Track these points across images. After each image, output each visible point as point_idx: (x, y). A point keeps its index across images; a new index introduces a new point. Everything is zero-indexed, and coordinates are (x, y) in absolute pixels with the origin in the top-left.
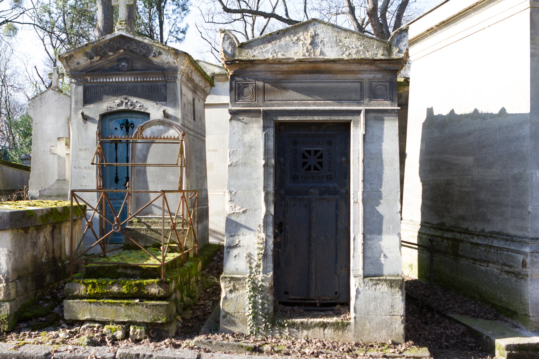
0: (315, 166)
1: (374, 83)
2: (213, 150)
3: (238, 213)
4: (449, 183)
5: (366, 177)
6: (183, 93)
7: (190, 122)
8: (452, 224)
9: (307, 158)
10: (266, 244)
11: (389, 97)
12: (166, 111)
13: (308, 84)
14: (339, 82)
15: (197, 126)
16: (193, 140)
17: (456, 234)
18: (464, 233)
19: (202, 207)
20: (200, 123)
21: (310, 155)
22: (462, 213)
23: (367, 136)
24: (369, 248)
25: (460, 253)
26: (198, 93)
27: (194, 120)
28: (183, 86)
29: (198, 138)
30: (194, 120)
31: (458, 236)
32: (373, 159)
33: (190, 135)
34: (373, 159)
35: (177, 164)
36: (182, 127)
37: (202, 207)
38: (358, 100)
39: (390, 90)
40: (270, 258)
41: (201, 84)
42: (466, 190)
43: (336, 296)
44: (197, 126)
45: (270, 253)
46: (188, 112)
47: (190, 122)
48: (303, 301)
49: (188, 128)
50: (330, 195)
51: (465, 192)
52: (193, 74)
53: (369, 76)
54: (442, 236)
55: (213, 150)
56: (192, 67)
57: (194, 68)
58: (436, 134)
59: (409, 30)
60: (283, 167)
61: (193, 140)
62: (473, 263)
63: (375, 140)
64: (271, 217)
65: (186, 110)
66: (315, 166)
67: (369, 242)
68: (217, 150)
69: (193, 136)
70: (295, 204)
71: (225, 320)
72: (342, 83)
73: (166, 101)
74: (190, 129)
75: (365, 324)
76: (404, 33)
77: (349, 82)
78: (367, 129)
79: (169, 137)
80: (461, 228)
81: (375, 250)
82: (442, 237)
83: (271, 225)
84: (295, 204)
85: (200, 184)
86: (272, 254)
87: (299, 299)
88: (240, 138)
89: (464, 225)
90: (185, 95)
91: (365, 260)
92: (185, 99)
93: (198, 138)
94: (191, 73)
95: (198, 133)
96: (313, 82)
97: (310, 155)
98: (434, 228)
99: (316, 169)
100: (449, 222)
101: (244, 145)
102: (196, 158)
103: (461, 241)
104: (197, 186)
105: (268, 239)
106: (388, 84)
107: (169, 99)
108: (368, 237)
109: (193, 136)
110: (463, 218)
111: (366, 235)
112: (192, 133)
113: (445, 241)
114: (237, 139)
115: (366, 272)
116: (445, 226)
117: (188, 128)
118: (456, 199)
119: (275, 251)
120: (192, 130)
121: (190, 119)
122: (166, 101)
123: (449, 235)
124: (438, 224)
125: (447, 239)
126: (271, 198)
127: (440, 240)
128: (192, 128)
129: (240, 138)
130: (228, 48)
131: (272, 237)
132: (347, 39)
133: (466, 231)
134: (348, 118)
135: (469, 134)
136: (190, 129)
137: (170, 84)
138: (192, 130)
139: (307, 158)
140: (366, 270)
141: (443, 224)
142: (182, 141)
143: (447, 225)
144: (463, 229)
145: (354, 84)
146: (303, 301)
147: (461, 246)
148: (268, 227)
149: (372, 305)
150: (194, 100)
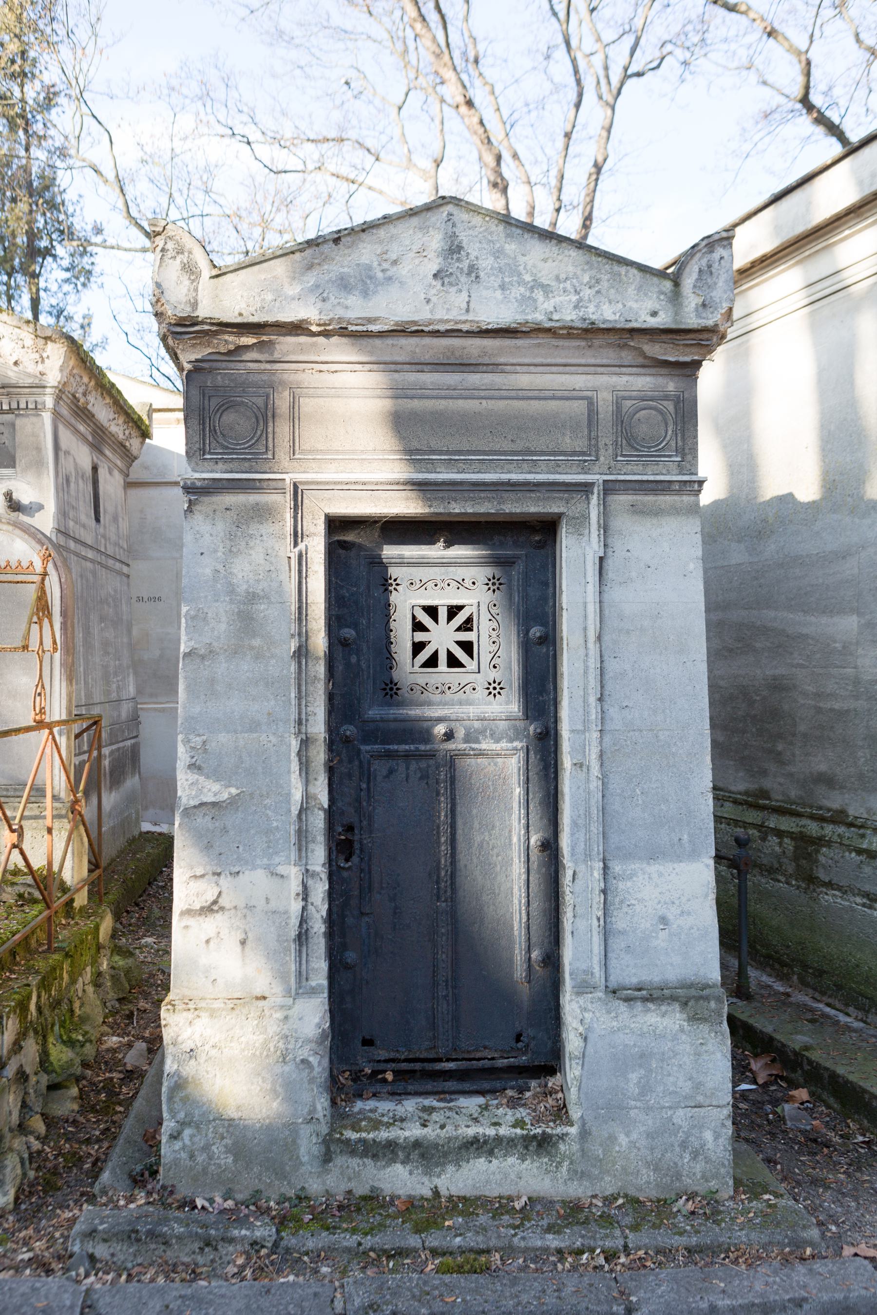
0: (450, 655)
1: (629, 403)
2: (150, 599)
3: (214, 804)
4: (778, 686)
5: (609, 687)
6: (64, 445)
7: (84, 526)
8: (793, 793)
9: (460, 643)
10: (305, 899)
11: (673, 443)
12: (15, 496)
13: (429, 404)
14: (523, 398)
15: (104, 536)
16: (94, 573)
17: (804, 821)
18: (833, 821)
19: (121, 745)
20: (113, 529)
21: (459, 629)
22: (823, 767)
23: (610, 564)
24: (622, 902)
25: (822, 875)
26: (107, 452)
27: (98, 520)
28: (61, 427)
29: (106, 567)
30: (98, 520)
31: (813, 828)
32: (628, 632)
33: (85, 558)
34: (628, 632)
35: (25, 648)
36: (62, 541)
37: (121, 745)
38: (583, 454)
39: (675, 423)
40: (319, 945)
41: (114, 429)
42: (837, 706)
43: (520, 1045)
44: (104, 536)
45: (318, 927)
46: (77, 499)
47: (84, 526)
48: (418, 1066)
49: (77, 541)
50: (497, 741)
51: (832, 710)
52: (91, 398)
53: (614, 379)
54: (762, 826)
55: (150, 599)
56: (86, 379)
57: (93, 383)
58: (738, 555)
59: (735, 242)
60: (354, 659)
61: (94, 573)
62: (864, 905)
63: (634, 574)
64: (321, 815)
65: (73, 493)
66: (450, 655)
67: (621, 885)
68: (159, 599)
69: (92, 561)
70: (391, 772)
71: (178, 1145)
72: (532, 402)
73: (14, 467)
74: (84, 544)
75: (612, 1138)
76: (720, 252)
77: (554, 398)
78: (609, 541)
79: (14, 564)
80: (820, 808)
81: (638, 908)
82: (760, 827)
83: (321, 838)
84: (391, 772)
85: (114, 686)
86: (323, 929)
87: (407, 1060)
88: (220, 567)
89: (834, 801)
90: (67, 453)
91: (610, 941)
92: (68, 465)
93: (106, 567)
94: (84, 394)
95: (108, 556)
96: (445, 398)
97: (459, 629)
98: (735, 802)
99: (453, 662)
100: (779, 786)
101: (231, 590)
102: (102, 619)
103: (820, 842)
104: (108, 692)
105: (310, 882)
106: (670, 406)
107: (21, 462)
108: (617, 867)
109: (92, 561)
110: (828, 781)
111: (610, 864)
112: (90, 554)
113: (773, 840)
114: (208, 571)
115: (612, 978)
116: (769, 799)
117: (77, 541)
118: (802, 728)
119: (333, 921)
120: (91, 547)
121: (83, 518)
122: (14, 467)
123: (786, 824)
124: (747, 793)
125: (780, 834)
126: (319, 755)
127: (757, 834)
128: (90, 543)
129: (220, 567)
130: (179, 283)
131: (324, 876)
132: (550, 264)
133: (839, 817)
134: (554, 508)
135: (844, 555)
136: (84, 544)
137: (25, 420)
138: (91, 547)
139: (460, 643)
140: (611, 971)
141: (764, 794)
142: (45, 574)
143: (774, 796)
144: (829, 810)
145: (568, 403)
146: (418, 1066)
147: (825, 855)
148: (311, 846)
149: (634, 1077)
150: (95, 469)
